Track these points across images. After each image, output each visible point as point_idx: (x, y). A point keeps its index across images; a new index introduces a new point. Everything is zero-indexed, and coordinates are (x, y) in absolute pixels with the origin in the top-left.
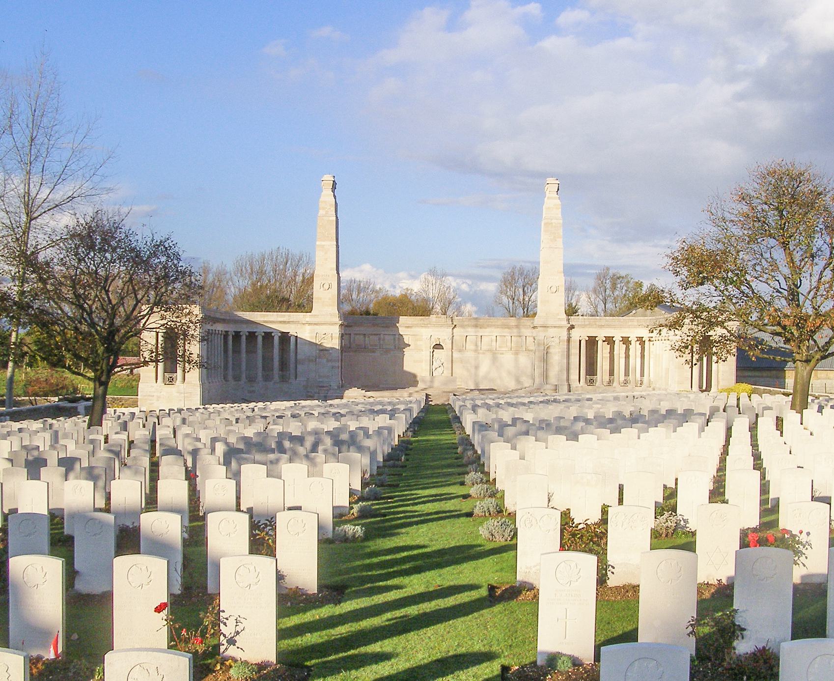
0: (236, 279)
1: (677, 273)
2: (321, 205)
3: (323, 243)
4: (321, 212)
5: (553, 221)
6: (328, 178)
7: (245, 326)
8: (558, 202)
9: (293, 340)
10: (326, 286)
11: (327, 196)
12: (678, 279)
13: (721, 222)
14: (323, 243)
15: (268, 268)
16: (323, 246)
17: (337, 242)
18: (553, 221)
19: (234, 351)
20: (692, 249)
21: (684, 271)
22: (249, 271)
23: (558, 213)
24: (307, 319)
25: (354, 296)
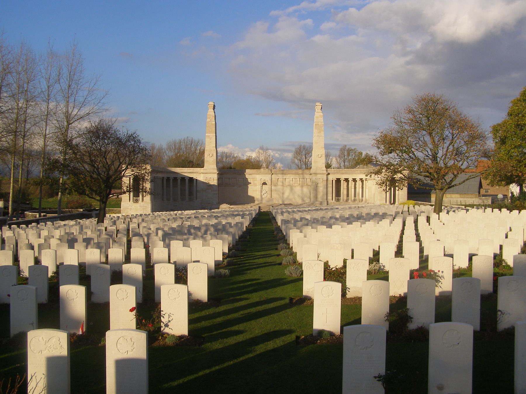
0: (167, 152)
1: (379, 148)
2: (208, 116)
4: (208, 120)
6: (211, 104)
8: (322, 114)
10: (211, 155)
11: (211, 112)
12: (379, 150)
13: (399, 123)
15: (183, 147)
23: (321, 119)
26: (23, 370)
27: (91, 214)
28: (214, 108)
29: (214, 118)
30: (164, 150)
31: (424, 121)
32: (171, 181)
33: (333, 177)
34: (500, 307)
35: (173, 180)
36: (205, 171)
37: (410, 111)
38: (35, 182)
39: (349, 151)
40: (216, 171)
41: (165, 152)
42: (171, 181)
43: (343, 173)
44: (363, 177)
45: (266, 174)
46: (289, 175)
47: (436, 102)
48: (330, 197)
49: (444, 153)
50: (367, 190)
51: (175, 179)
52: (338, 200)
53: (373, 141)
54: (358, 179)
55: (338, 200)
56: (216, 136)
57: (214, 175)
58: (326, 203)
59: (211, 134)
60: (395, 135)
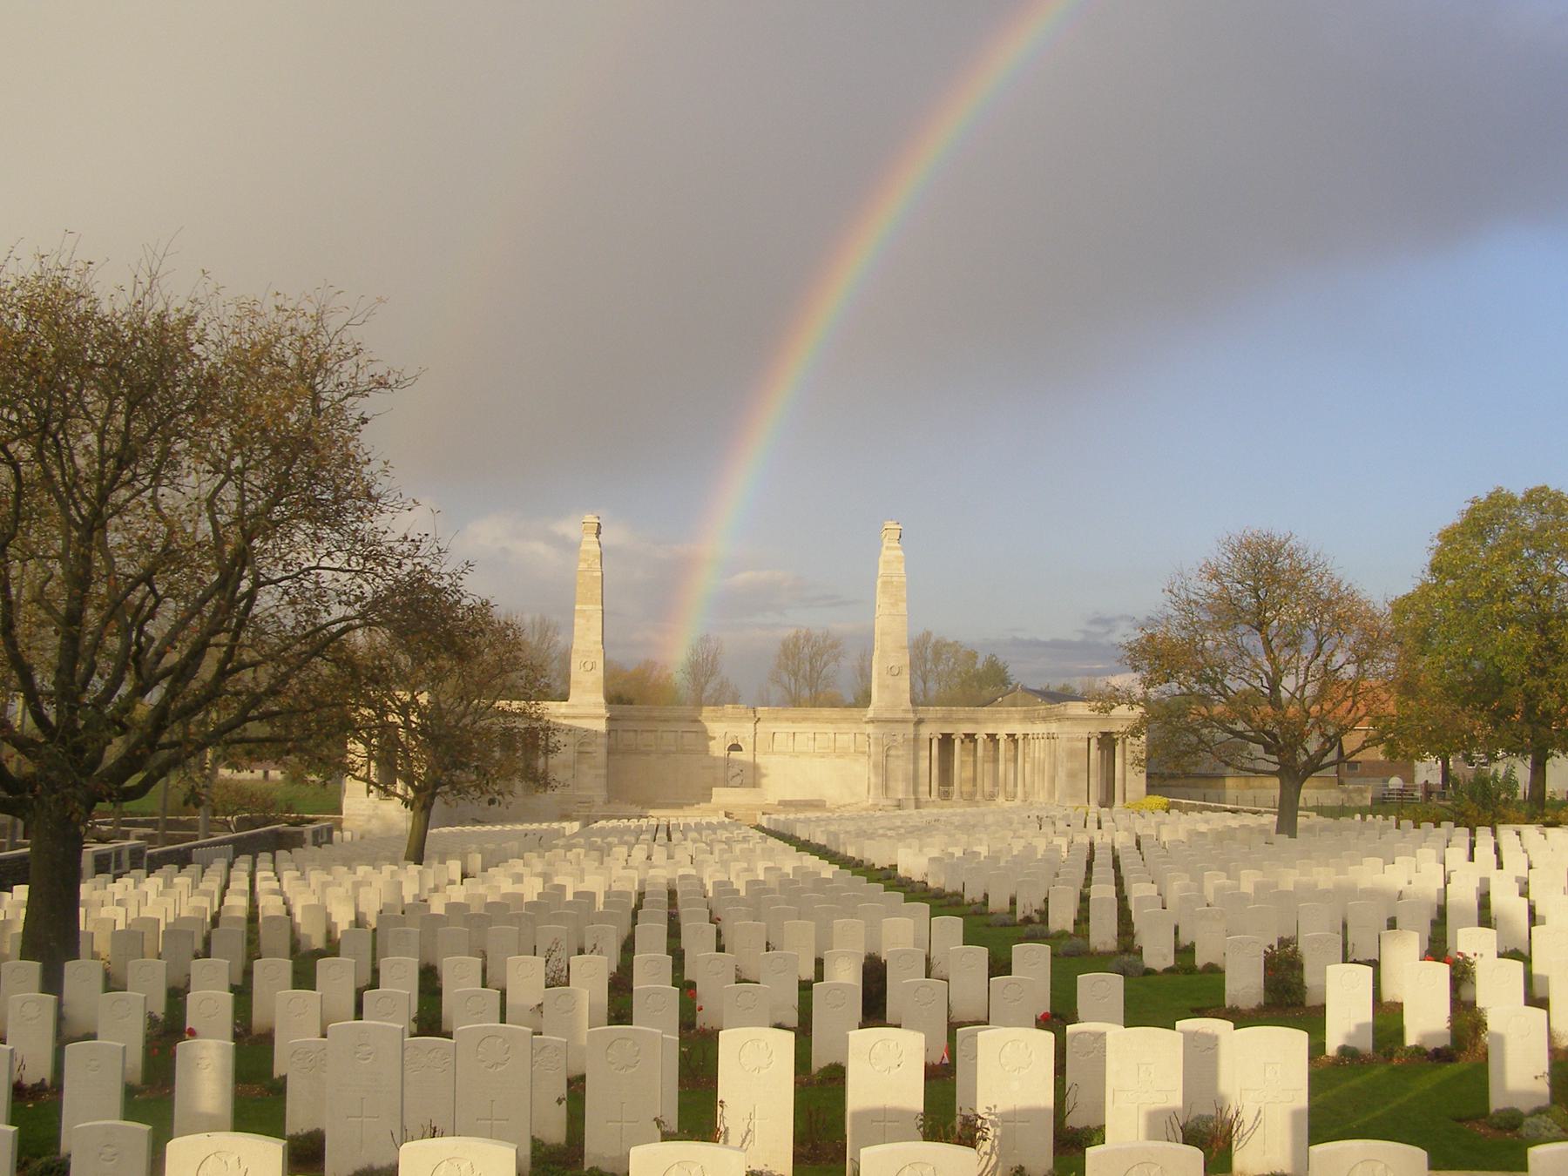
2: (582, 556)
4: (582, 566)
8: (901, 553)
26: (844, 1130)
27: (301, 833)
31: (1249, 601)
33: (930, 731)
34: (721, 1095)
36: (571, 711)
37: (1216, 576)
39: (940, 649)
43: (960, 720)
44: (1018, 729)
45: (740, 719)
46: (804, 725)
47: (1275, 551)
48: (924, 788)
49: (1301, 682)
50: (1028, 766)
52: (946, 795)
54: (1002, 736)
55: (946, 795)
57: (596, 722)
58: (912, 803)
59: (591, 607)
60: (1176, 634)
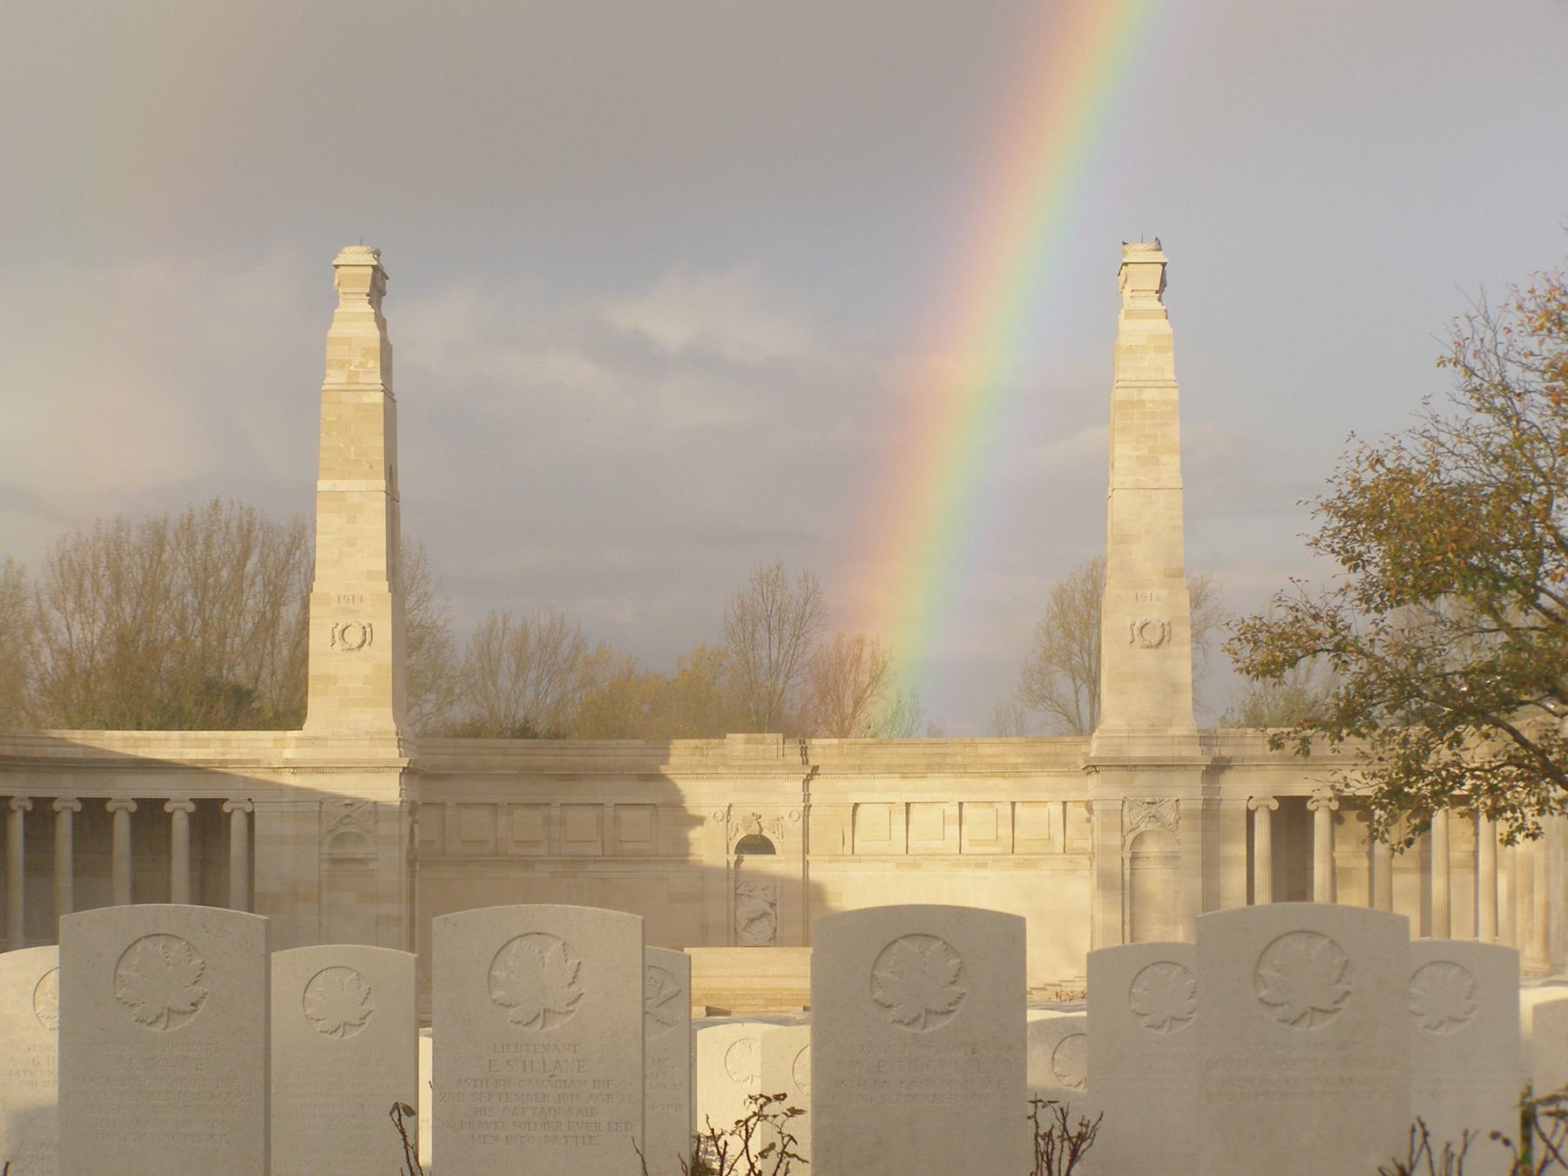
0: (56, 618)
1: (1354, 561)
2: (332, 352)
3: (342, 485)
4: (334, 378)
5: (1148, 394)
6: (357, 256)
7: (67, 780)
8: (1163, 326)
9: (237, 824)
10: (354, 637)
11: (353, 321)
12: (1356, 578)
13: (1496, 396)
14: (342, 485)
15: (179, 578)
16: (340, 495)
17: (391, 474)
18: (1148, 394)
19: (30, 869)
20: (1402, 479)
21: (1375, 552)
22: (108, 591)
23: (1164, 365)
24: (289, 753)
25: (504, 682)
28: (377, 293)
29: (374, 365)
30: (30, 606)
32: (64, 826)
35: (135, 818)
38: (1231, 767)
40: (391, 753)
41: (42, 620)
42: (64, 826)
51: (151, 814)
53: (1323, 518)
56: (392, 497)
